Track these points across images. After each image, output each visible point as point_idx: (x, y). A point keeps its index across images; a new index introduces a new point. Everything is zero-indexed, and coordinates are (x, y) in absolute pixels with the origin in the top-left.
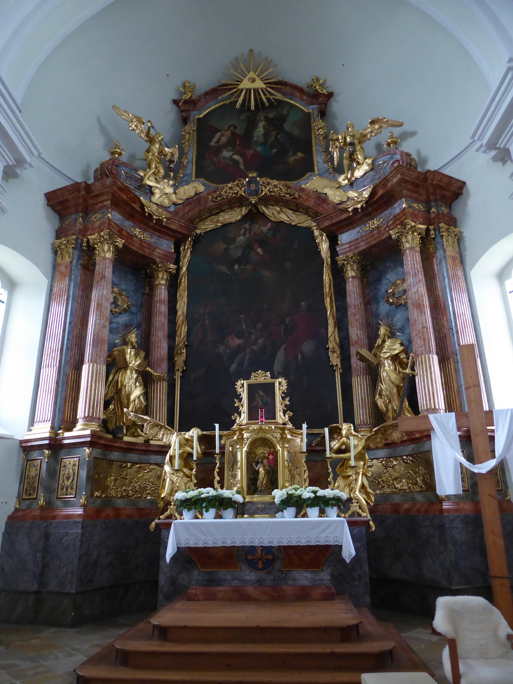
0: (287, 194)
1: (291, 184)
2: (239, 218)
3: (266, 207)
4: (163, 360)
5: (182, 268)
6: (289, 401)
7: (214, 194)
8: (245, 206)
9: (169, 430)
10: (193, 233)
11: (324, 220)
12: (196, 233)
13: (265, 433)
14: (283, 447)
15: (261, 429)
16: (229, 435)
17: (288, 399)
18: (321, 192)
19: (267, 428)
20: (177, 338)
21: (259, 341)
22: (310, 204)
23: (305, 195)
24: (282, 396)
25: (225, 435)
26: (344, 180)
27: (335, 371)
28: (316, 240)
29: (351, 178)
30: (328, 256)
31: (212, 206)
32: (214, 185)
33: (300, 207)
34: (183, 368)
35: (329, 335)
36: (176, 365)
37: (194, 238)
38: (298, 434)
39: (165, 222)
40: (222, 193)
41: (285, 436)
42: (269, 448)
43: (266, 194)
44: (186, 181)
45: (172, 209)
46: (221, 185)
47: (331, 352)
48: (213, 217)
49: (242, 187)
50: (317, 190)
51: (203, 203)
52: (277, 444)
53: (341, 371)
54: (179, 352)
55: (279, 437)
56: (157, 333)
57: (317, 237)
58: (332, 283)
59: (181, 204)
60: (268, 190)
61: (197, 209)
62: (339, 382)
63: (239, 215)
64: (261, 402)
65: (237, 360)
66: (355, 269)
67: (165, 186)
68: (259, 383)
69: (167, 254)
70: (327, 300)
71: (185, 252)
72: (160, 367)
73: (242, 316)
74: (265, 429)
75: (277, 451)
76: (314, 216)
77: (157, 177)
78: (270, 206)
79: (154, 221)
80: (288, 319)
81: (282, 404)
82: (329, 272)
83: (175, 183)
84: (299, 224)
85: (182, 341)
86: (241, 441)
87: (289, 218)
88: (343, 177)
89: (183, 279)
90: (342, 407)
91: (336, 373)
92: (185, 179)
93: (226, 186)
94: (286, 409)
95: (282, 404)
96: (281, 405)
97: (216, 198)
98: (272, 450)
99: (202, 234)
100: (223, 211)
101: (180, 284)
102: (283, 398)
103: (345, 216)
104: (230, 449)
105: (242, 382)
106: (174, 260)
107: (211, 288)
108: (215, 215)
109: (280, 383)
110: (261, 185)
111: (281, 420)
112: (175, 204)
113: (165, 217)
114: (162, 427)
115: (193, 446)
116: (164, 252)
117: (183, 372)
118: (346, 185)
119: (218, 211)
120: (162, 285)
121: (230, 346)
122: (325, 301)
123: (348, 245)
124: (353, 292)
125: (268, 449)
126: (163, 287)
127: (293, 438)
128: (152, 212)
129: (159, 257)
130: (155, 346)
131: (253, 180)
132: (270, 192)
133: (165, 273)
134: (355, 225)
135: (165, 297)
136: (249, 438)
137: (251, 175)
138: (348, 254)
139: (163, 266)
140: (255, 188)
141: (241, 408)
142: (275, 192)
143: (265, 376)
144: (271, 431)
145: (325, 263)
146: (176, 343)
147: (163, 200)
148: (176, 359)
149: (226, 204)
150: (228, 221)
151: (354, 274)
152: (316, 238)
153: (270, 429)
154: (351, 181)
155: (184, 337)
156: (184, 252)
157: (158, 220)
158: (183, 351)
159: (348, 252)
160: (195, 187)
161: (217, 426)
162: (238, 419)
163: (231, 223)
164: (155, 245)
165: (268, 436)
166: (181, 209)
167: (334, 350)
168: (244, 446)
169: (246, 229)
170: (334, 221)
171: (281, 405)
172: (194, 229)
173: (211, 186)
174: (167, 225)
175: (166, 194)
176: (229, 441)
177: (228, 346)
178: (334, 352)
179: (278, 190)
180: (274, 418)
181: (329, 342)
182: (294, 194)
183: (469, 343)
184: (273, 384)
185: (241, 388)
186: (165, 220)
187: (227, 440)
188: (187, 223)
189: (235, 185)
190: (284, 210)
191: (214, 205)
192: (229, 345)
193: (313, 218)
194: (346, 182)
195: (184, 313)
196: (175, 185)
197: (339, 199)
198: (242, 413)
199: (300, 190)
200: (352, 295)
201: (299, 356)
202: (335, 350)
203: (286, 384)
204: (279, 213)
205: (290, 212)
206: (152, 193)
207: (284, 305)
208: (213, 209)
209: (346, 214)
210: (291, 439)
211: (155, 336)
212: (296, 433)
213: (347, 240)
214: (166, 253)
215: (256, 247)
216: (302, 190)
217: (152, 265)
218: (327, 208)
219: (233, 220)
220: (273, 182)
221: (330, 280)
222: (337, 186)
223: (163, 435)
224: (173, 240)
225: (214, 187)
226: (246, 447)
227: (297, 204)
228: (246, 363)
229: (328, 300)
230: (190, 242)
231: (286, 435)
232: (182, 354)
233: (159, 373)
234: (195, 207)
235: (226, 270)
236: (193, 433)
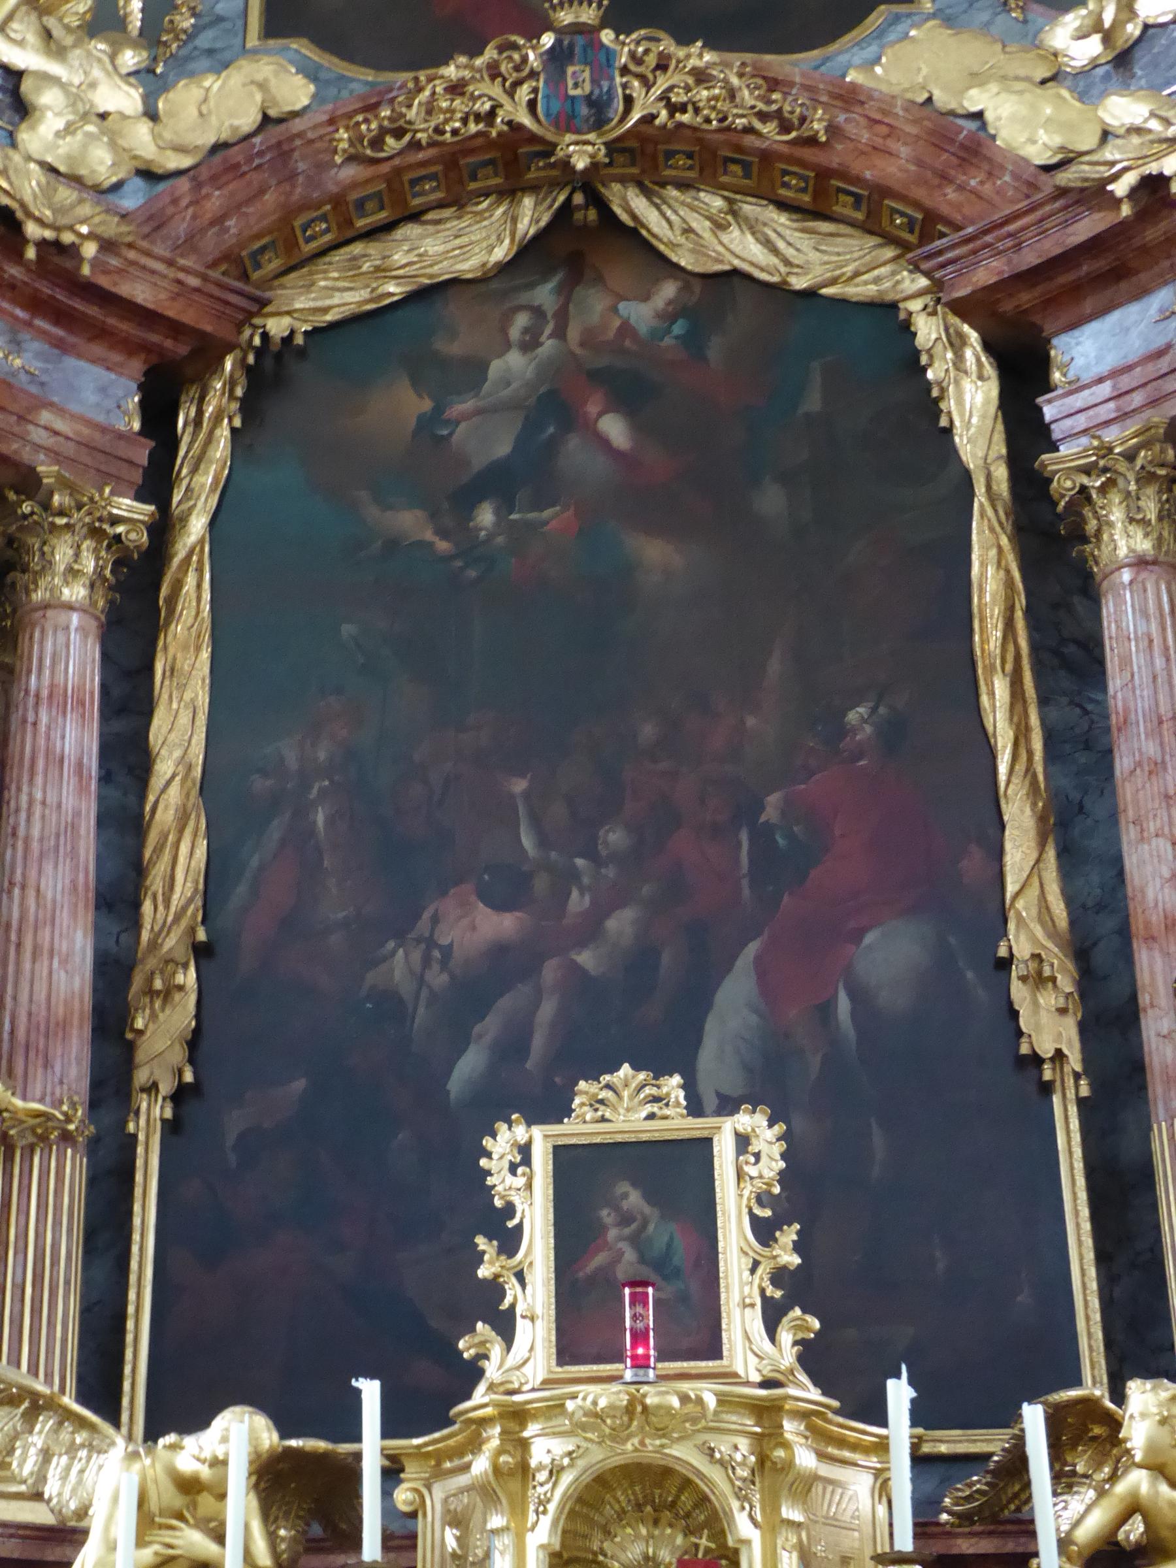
0: (763, 117)
1: (788, 68)
2: (500, 253)
3: (647, 193)
4: (64, 1025)
5: (184, 519)
6: (798, 1247)
7: (366, 121)
8: (533, 188)
9: (82, 1423)
10: (247, 332)
11: (975, 252)
12: (265, 336)
13: (661, 1432)
14: (772, 1525)
15: (635, 1409)
16: (439, 1457)
17: (789, 1235)
18: (953, 105)
19: (675, 1402)
20: (147, 907)
21: (612, 924)
22: (892, 169)
23: (863, 121)
24: (753, 1218)
25: (419, 1454)
26: (1082, 35)
27: (1047, 1089)
28: (924, 370)
29: (1117, 24)
30: (992, 455)
31: (354, 185)
32: (369, 76)
33: (839, 190)
34: (180, 1072)
35: (1011, 888)
36: (140, 1056)
37: (251, 359)
38: (855, 1447)
39: (95, 263)
40: (412, 114)
41: (780, 1453)
42: (688, 1532)
43: (649, 119)
44: (210, 52)
45: (133, 199)
46: (405, 76)
47: (1023, 979)
48: (357, 248)
49: (518, 83)
50: (930, 100)
51: (301, 166)
52: (735, 1504)
53: (1085, 1091)
54: (158, 984)
55: (743, 1464)
56: (33, 873)
57: (929, 351)
58: (1021, 601)
59: (179, 173)
60: (660, 98)
61: (269, 197)
62: (1078, 1152)
63: (500, 240)
64: (630, 1255)
65: (490, 1027)
66: (1152, 516)
67: (96, 73)
68: (619, 1138)
69: (99, 439)
70: (992, 694)
71: (202, 436)
72: (47, 1064)
73: (519, 786)
74: (659, 1407)
75: (736, 1552)
76: (912, 239)
77: (51, 22)
78: (672, 192)
79: (31, 253)
80: (773, 800)
81: (756, 1265)
82: (1004, 541)
83: (155, 59)
84: (833, 282)
85: (177, 918)
86: (514, 1485)
87: (775, 251)
88: (1077, 23)
89: (191, 580)
90: (1095, 1303)
91: (1056, 1099)
92: (204, 40)
93: (430, 80)
94: (778, 1294)
95: (756, 1265)
96: (753, 1271)
97: (377, 142)
98: (704, 1542)
99: (299, 340)
100: (415, 217)
101: (171, 610)
102: (764, 1231)
103: (1087, 226)
104: (450, 1538)
105: (521, 1132)
106: (137, 477)
107: (348, 630)
108: (370, 234)
109: (743, 1141)
110: (625, 70)
111: (753, 1361)
112: (148, 174)
113: (91, 236)
114: (37, 1406)
115: (223, 1524)
116: (86, 431)
117: (179, 1096)
118: (1094, 64)
119: (383, 215)
120: (70, 607)
121: (447, 951)
122: (985, 699)
123: (1106, 389)
124: (1144, 644)
125: (679, 1540)
126: (75, 619)
127: (826, 1470)
128: (23, 205)
129: (55, 456)
130: (19, 945)
131: (580, 41)
132: (673, 109)
133: (87, 544)
134: (1143, 277)
135: (83, 676)
136: (562, 1469)
137: (565, 17)
138: (1111, 435)
139: (79, 507)
140: (587, 87)
141: (512, 1289)
142: (697, 110)
143: (656, 1099)
144: (694, 1420)
145: (980, 489)
146: (145, 936)
147: (85, 147)
148: (139, 1024)
149: (432, 177)
150: (443, 271)
151: (1144, 545)
152: (924, 359)
153: (690, 1408)
154: (1121, 44)
155: (190, 901)
156: (195, 435)
157: (52, 248)
158: (180, 979)
159: (1107, 423)
160: (262, 86)
161: (370, 1391)
162: (496, 1351)
163: (455, 282)
164: (34, 389)
165: (677, 1451)
166: (184, 202)
167: (1039, 973)
168: (532, 1517)
169: (538, 312)
170: (1030, 258)
171: (753, 1271)
172: (254, 308)
173: (352, 80)
174: (104, 281)
175: (103, 116)
176: (439, 1491)
177: (440, 947)
178: (1039, 980)
179: (716, 98)
180: (714, 1350)
181: (1012, 926)
182: (803, 119)
183: (887, 1550)
184: (706, 1143)
185: (513, 1169)
186: (90, 250)
187: (429, 1487)
188: (215, 274)
189: (480, 71)
190: (747, 208)
191: (368, 181)
192: (444, 941)
193: (905, 247)
194: (1093, 47)
195: (190, 768)
196: (151, 71)
197: (1057, 140)
198: (520, 1322)
199: (839, 97)
200: (1138, 660)
201: (844, 1004)
202: (1047, 972)
203: (777, 1149)
204: (719, 226)
205: (783, 219)
206: (22, 109)
207: (751, 721)
208: (360, 205)
209: (1097, 216)
210: (816, 1478)
211: (23, 887)
212: (842, 1443)
213: (1099, 359)
214: (97, 436)
215: (592, 409)
216: (850, 97)
217: (12, 496)
218: (987, 189)
219: (468, 266)
220: (688, 56)
221: (1009, 584)
222: (1043, 72)
223: (46, 1456)
224: (137, 366)
225: (367, 83)
226: (546, 1522)
227: (824, 174)
228: (538, 1042)
229: (1001, 688)
230: (232, 383)
231: (786, 1445)
232: (177, 996)
233: (41, 1100)
234: (262, 191)
235: (429, 535)
236: (225, 1440)
